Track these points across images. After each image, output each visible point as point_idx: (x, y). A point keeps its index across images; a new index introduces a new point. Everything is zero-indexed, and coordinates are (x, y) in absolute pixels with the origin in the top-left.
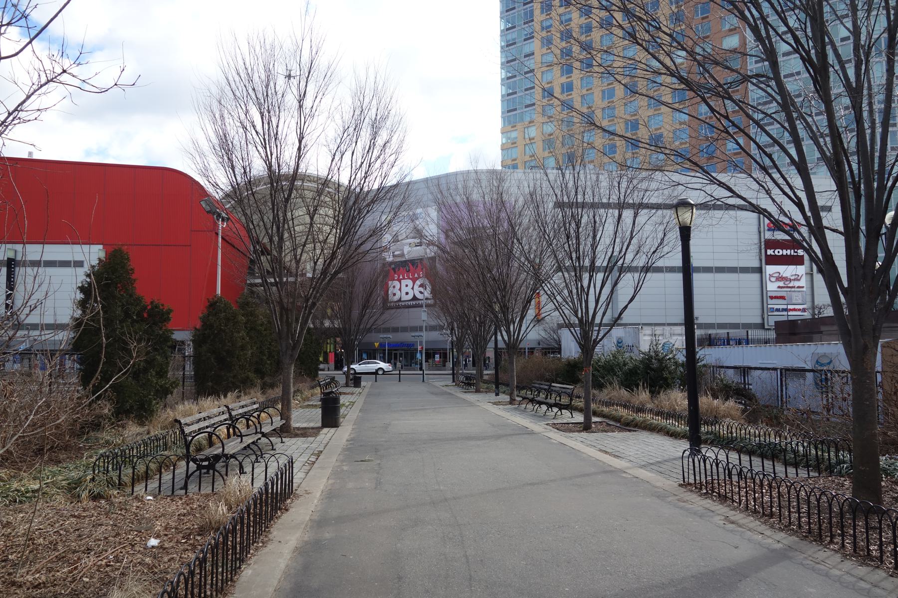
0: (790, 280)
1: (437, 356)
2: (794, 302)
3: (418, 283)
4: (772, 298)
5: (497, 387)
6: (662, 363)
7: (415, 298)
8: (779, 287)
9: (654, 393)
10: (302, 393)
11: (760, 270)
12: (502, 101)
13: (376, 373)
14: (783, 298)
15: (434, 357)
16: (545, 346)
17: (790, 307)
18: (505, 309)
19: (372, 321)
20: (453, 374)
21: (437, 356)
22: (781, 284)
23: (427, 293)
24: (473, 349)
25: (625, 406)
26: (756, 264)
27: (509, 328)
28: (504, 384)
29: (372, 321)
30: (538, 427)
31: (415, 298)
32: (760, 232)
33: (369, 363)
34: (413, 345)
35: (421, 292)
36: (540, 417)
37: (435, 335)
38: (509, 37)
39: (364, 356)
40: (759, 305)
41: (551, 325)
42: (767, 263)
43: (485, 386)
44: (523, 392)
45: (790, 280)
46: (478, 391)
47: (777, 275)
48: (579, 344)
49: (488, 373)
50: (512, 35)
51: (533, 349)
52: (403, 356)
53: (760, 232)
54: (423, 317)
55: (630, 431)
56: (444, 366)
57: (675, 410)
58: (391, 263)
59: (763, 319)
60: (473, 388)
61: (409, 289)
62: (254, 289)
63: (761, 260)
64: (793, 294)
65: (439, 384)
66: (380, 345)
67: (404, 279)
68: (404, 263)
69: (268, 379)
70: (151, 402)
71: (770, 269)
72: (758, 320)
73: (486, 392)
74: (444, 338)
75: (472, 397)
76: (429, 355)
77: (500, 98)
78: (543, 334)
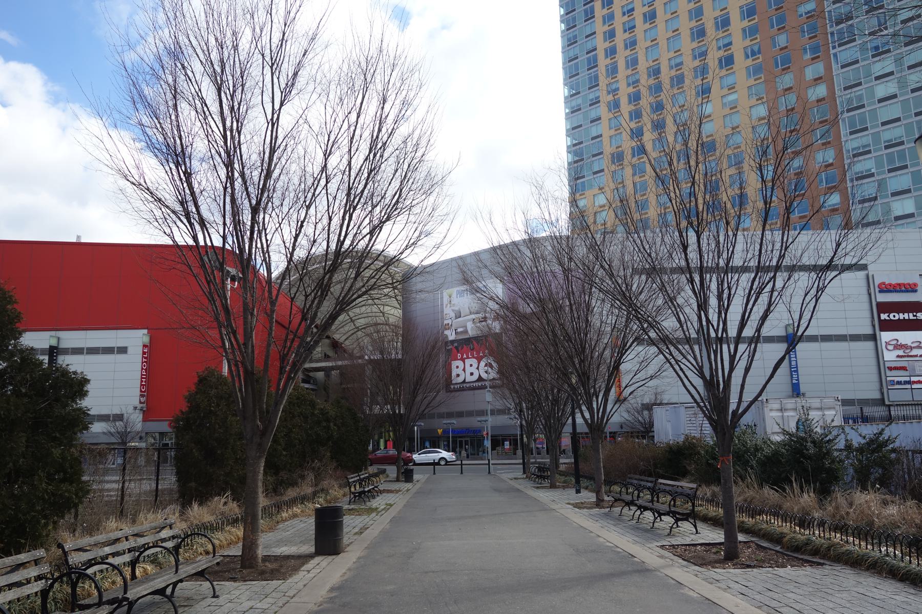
0: (911, 348)
1: (507, 444)
2: (918, 373)
3: (482, 364)
4: (890, 369)
5: (578, 482)
6: (821, 448)
7: (480, 379)
8: (898, 356)
9: (824, 492)
10: (327, 493)
11: (873, 338)
12: (562, 37)
13: (435, 464)
14: (904, 368)
15: (503, 444)
16: (629, 430)
17: (913, 379)
18: (584, 378)
19: (426, 402)
20: (524, 464)
21: (507, 444)
22: (901, 353)
23: (493, 374)
24: (546, 435)
25: (776, 515)
26: (868, 331)
27: (592, 405)
28: (586, 477)
29: (426, 402)
30: (648, 553)
31: (480, 379)
32: (870, 295)
33: (429, 452)
34: (480, 431)
35: (486, 372)
36: (646, 531)
37: (502, 420)
38: (574, 103)
39: (427, 444)
40: (875, 378)
41: (635, 405)
42: (882, 330)
43: (563, 478)
44: (616, 488)
45: (911, 348)
46: (553, 486)
47: (895, 342)
48: (710, 419)
49: (566, 461)
50: (578, 101)
51: (615, 433)
52: (467, 443)
53: (870, 295)
54: (488, 397)
55: (812, 564)
56: (515, 454)
57: (871, 524)
58: (452, 342)
59: (882, 394)
60: (546, 483)
61: (473, 369)
62: (311, 374)
63: (874, 326)
64: (916, 363)
65: (506, 476)
66: (444, 432)
67: (468, 358)
68: (468, 341)
69: (284, 475)
70: (38, 522)
71: (886, 336)
72: (876, 395)
73: (564, 488)
74: (510, 422)
75: (544, 496)
76: (497, 442)
77: (563, 100)
78: (626, 415)
